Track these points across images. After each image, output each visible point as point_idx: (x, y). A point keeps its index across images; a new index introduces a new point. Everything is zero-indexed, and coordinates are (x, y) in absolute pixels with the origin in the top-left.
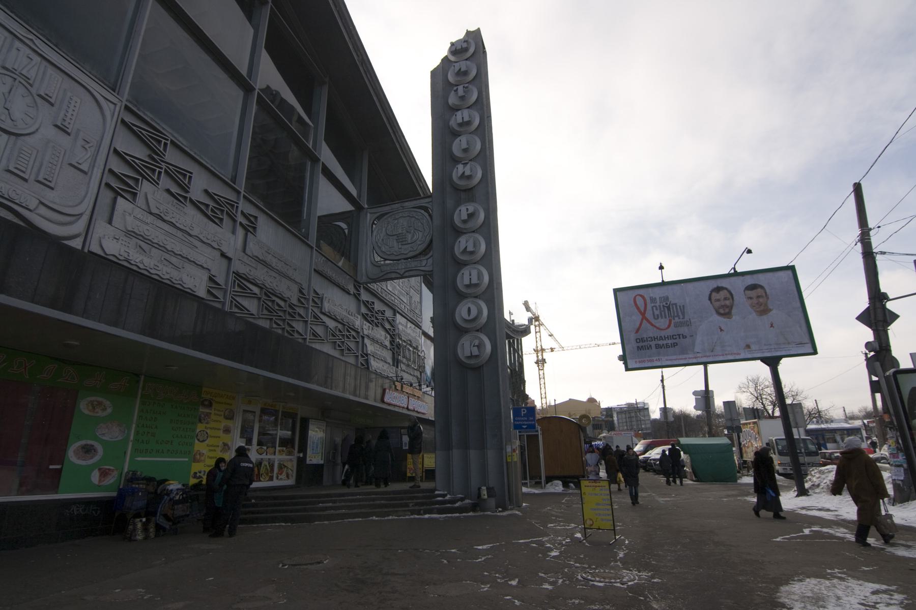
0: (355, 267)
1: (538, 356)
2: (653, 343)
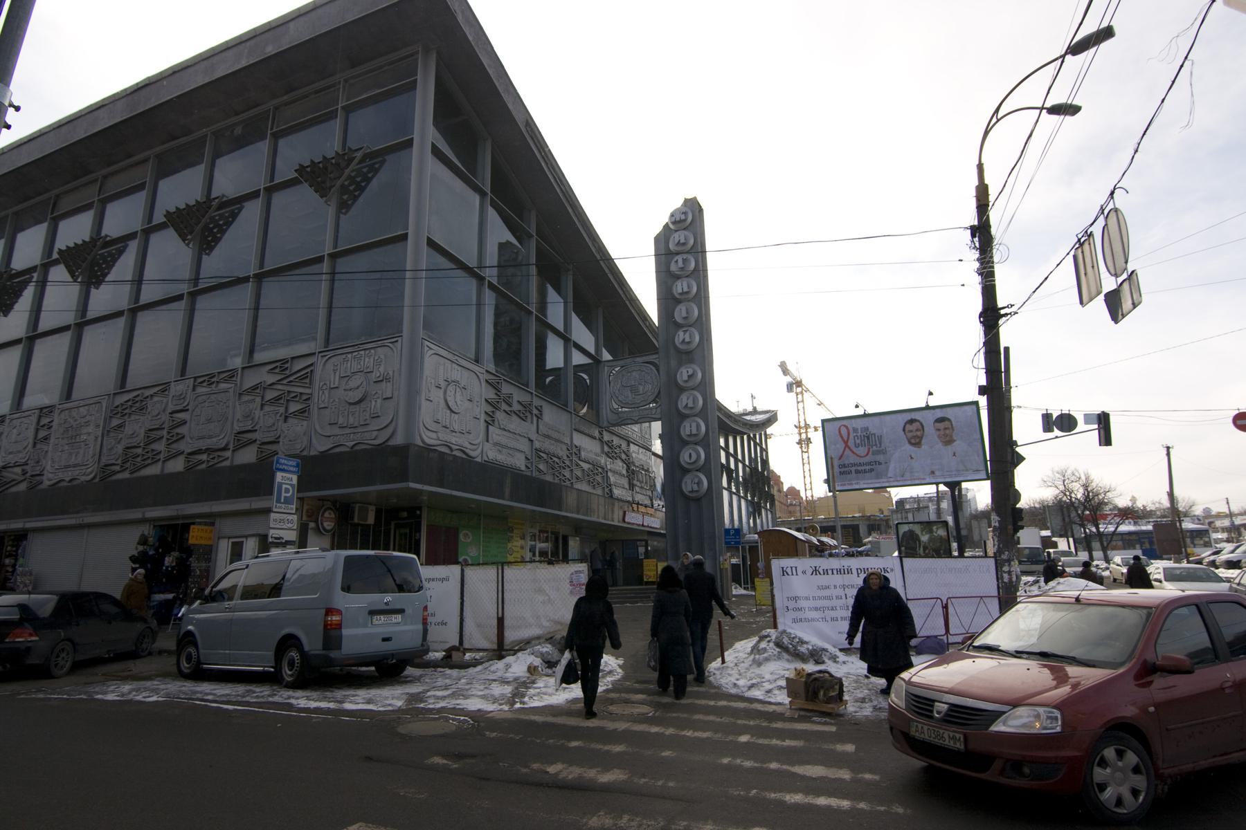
2: (853, 469)
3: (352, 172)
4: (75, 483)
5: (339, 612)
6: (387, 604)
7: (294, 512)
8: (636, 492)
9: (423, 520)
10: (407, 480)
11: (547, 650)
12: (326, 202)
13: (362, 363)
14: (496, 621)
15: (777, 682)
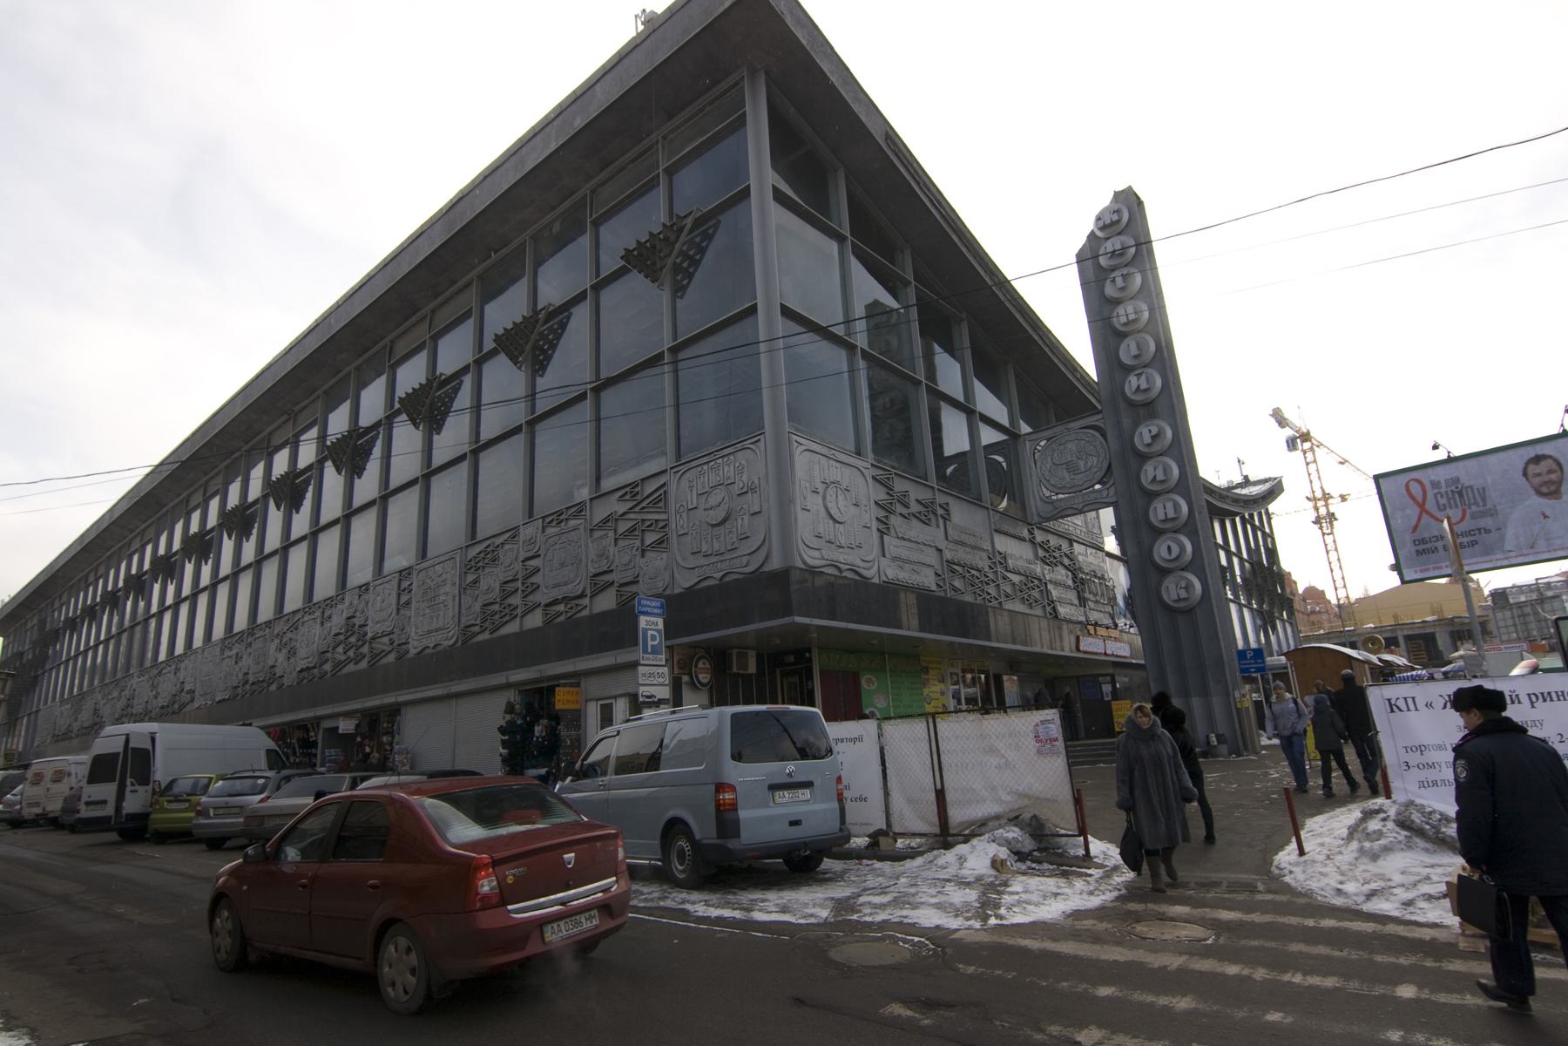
0: (1023, 506)
1: (1316, 509)
3: (684, 244)
4: (438, 649)
5: (732, 788)
6: (790, 775)
7: (664, 663)
8: (1090, 609)
9: (814, 662)
10: (790, 614)
11: (1015, 835)
12: (658, 287)
13: (721, 474)
14: (934, 794)
15: (1419, 887)
